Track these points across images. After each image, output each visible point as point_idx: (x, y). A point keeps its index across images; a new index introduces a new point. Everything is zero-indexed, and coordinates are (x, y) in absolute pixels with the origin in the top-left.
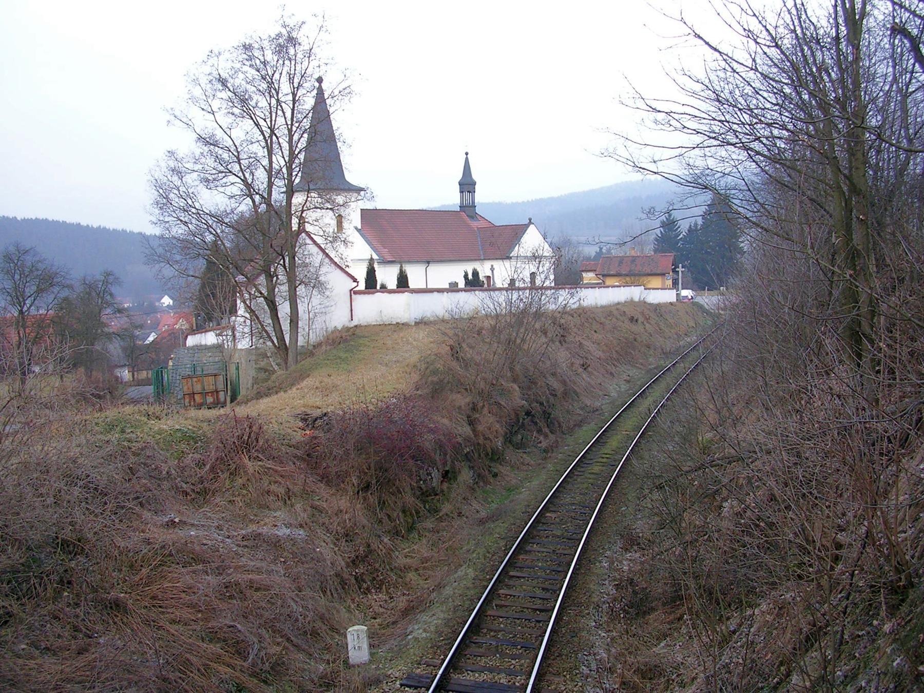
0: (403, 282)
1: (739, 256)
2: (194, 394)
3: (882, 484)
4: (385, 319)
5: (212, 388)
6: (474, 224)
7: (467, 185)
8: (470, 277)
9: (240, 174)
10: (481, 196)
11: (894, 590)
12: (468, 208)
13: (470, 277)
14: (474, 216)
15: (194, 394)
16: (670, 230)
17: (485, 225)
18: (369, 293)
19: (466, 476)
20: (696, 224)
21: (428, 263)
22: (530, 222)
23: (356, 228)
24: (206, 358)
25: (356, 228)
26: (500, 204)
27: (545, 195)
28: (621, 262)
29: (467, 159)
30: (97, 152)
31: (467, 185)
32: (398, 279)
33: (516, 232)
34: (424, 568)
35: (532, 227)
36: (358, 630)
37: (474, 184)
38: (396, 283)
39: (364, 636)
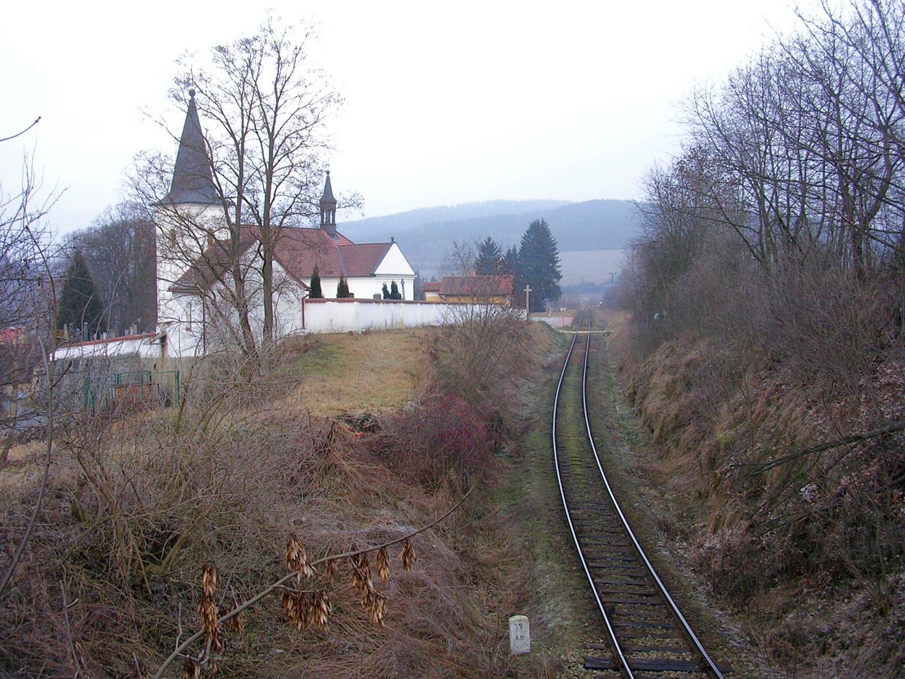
0: (344, 294)
1: (555, 280)
3: (164, 492)
4: (335, 328)
8: (389, 290)
10: (341, 217)
11: (843, 645)
13: (389, 290)
16: (490, 254)
18: (340, 302)
20: (514, 250)
22: (393, 242)
27: (613, 197)
28: (462, 283)
30: (82, 174)
32: (339, 289)
33: (379, 251)
34: (503, 563)
35: (394, 246)
36: (520, 620)
38: (336, 292)
39: (527, 626)
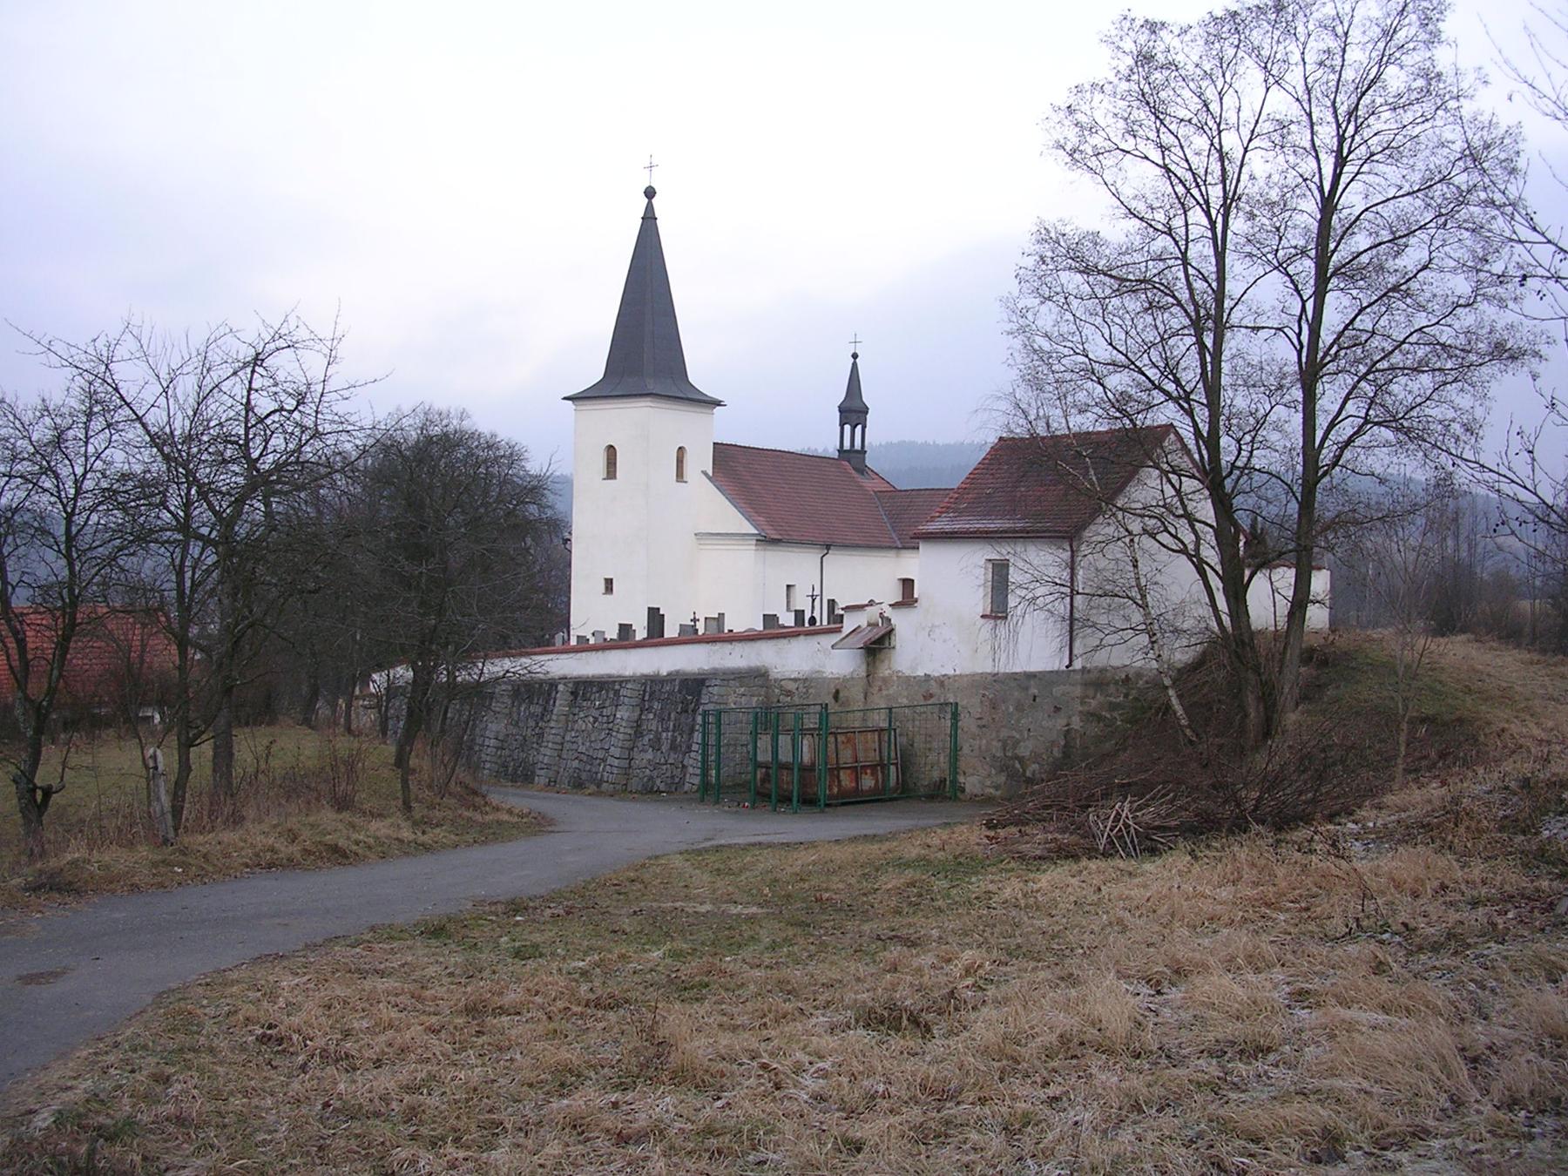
2: (839, 769)
5: (874, 757)
6: (868, 484)
7: (853, 412)
9: (1182, 243)
10: (878, 433)
12: (852, 457)
14: (862, 469)
15: (839, 769)
17: (884, 487)
19: (1030, 1050)
21: (828, 547)
23: (705, 473)
24: (736, 698)
25: (705, 473)
26: (902, 444)
29: (855, 366)
30: (43, 386)
31: (853, 412)
37: (865, 411)
